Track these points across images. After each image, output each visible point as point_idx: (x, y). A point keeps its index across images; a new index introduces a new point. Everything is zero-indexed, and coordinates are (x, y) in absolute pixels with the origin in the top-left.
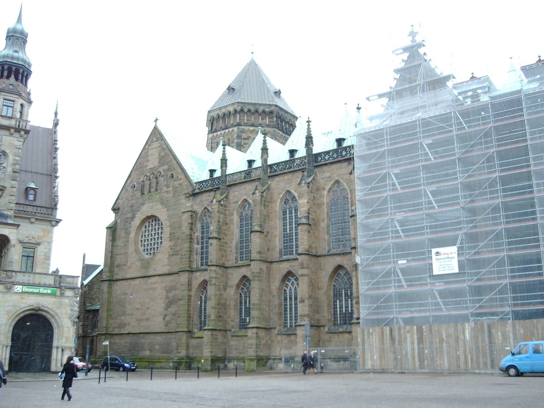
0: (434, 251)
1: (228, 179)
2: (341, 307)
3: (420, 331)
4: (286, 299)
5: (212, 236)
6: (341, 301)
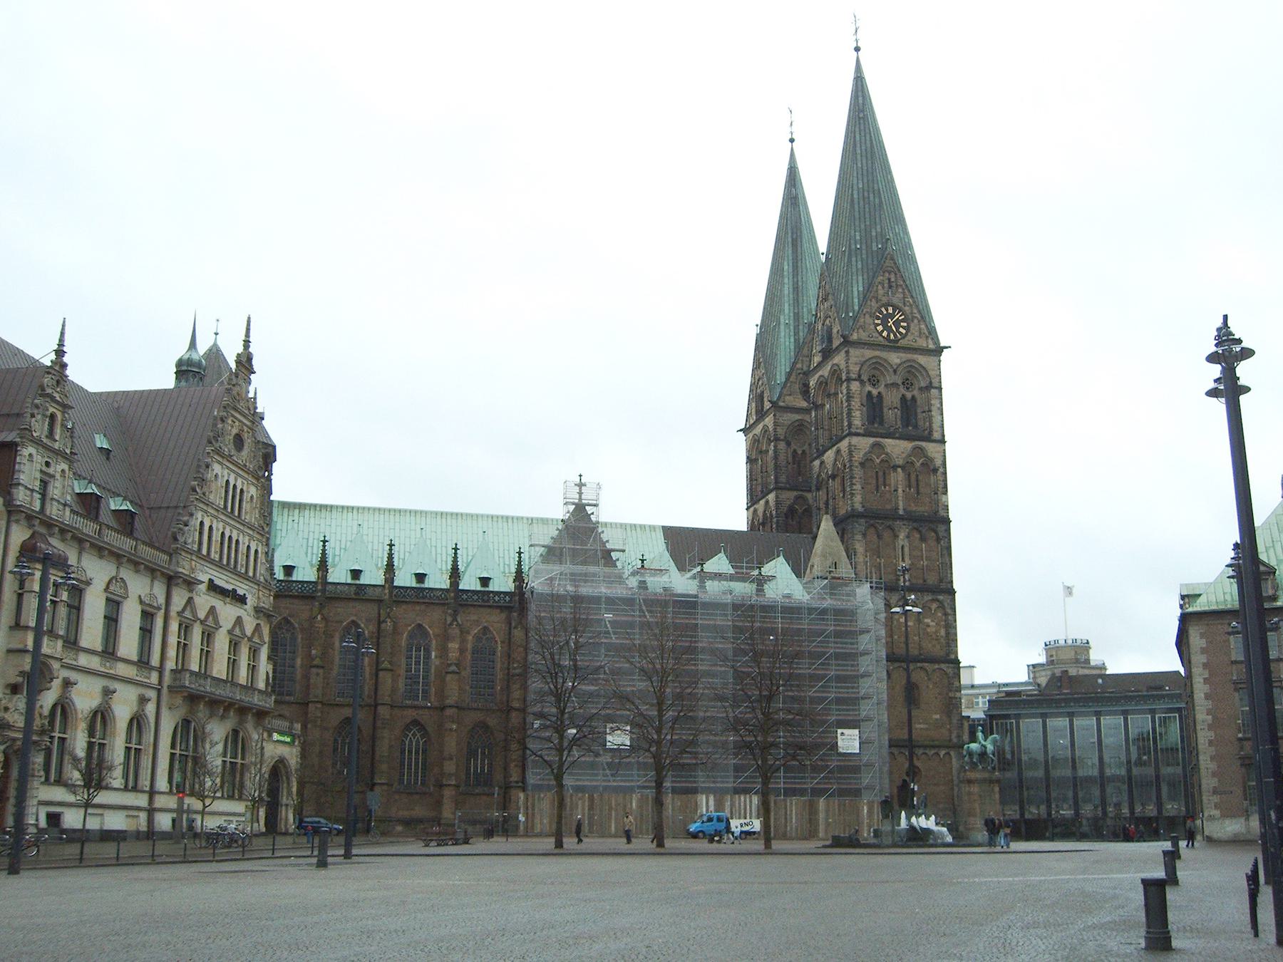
0: (840, 731)
1: (329, 588)
2: (476, 767)
3: (591, 799)
4: (403, 752)
5: (315, 663)
6: (476, 760)
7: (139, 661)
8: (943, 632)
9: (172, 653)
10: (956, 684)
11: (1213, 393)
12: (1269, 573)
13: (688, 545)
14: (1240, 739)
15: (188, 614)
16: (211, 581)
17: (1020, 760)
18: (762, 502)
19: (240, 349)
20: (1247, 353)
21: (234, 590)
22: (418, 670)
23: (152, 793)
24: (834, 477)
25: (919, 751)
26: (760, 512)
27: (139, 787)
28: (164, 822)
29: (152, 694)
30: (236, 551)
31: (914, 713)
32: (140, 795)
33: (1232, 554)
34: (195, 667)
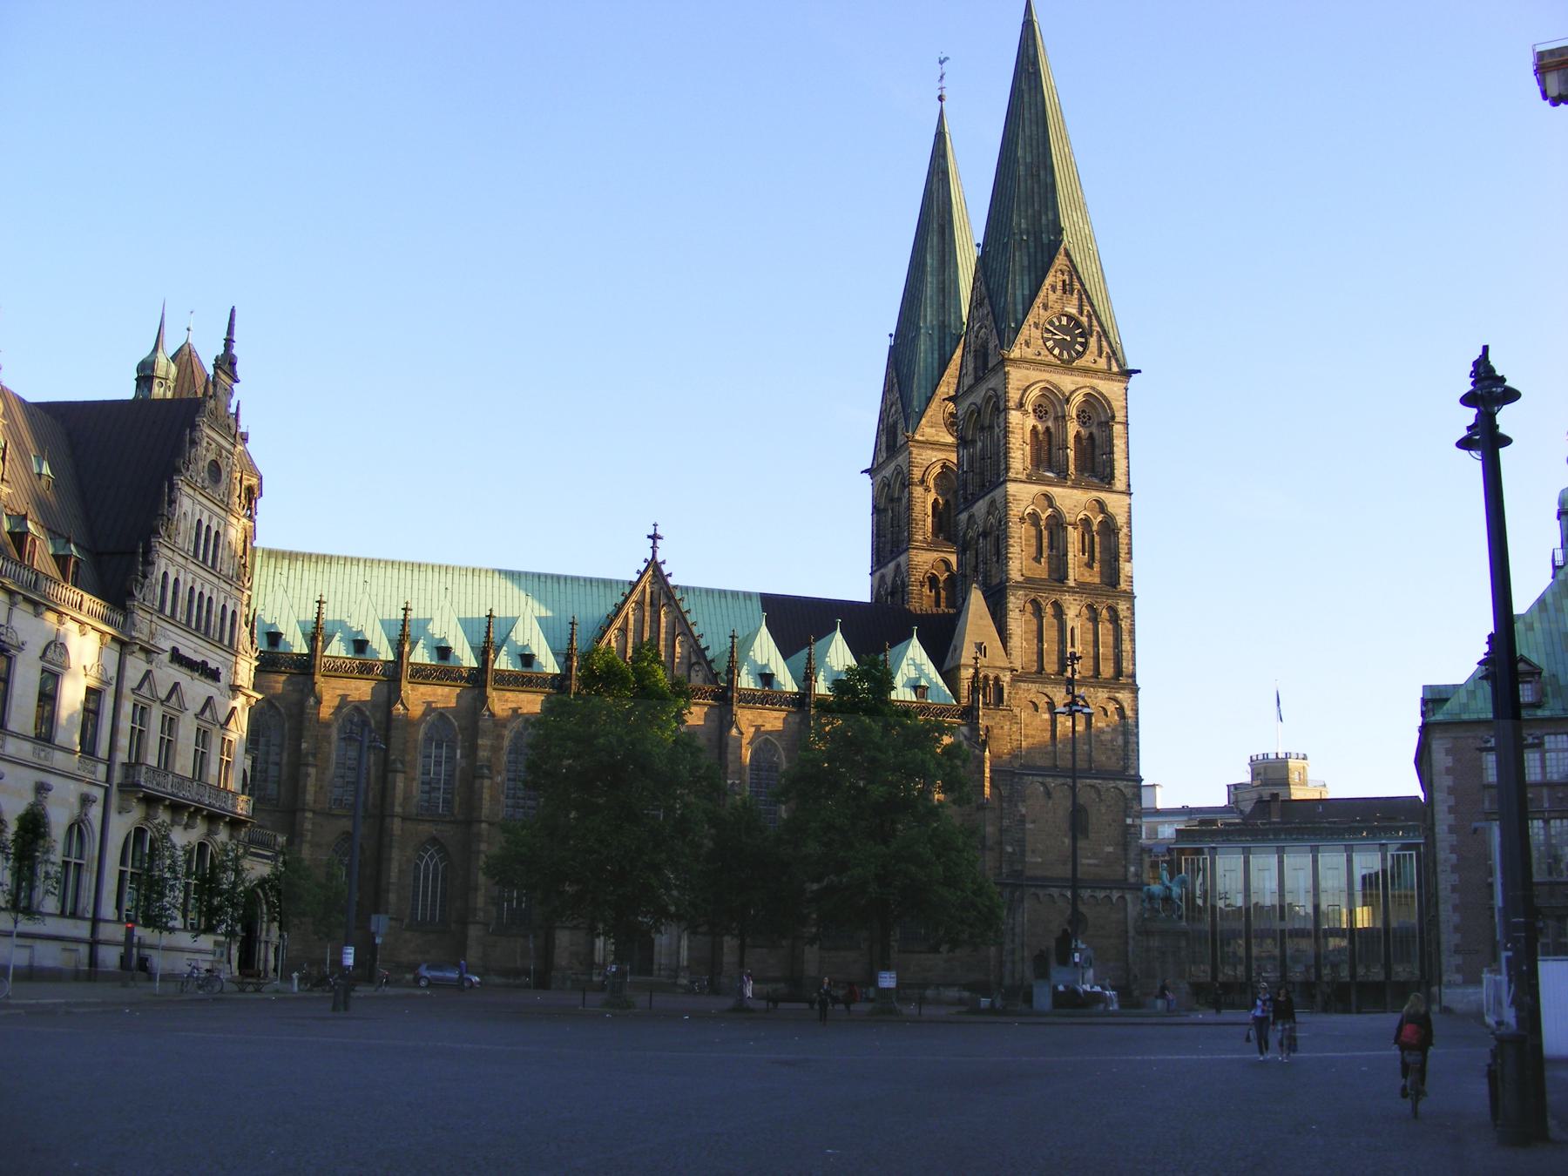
4: (416, 878)
7: (38, 737)
8: (1120, 740)
9: (124, 741)
10: (1136, 808)
11: (1463, 444)
12: (1532, 674)
13: (797, 621)
15: (145, 690)
16: (175, 650)
17: (1214, 907)
18: (892, 565)
19: (221, 351)
20: (1512, 395)
21: (204, 663)
22: (438, 774)
23: (96, 920)
24: (985, 534)
25: (1086, 893)
26: (889, 580)
27: (79, 912)
28: (110, 957)
29: (98, 793)
30: (209, 612)
31: (1081, 843)
32: (79, 922)
33: (1486, 649)
34: (152, 760)
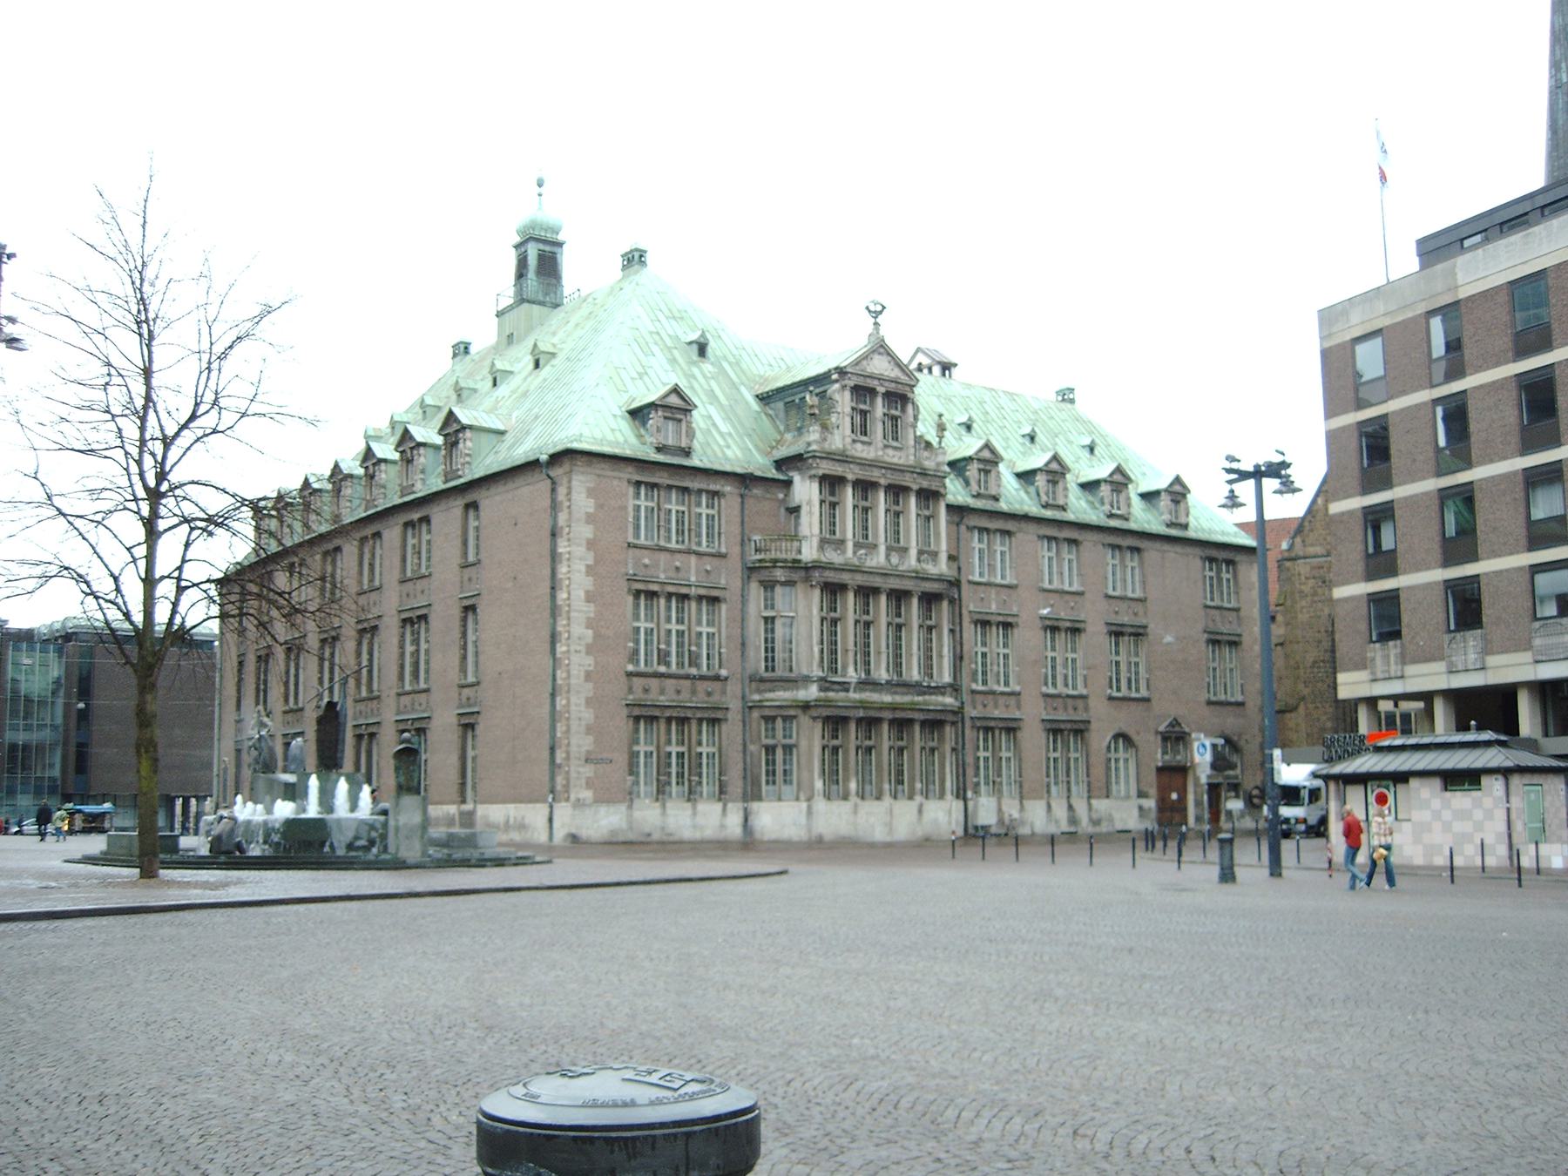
14: (630, 675)
